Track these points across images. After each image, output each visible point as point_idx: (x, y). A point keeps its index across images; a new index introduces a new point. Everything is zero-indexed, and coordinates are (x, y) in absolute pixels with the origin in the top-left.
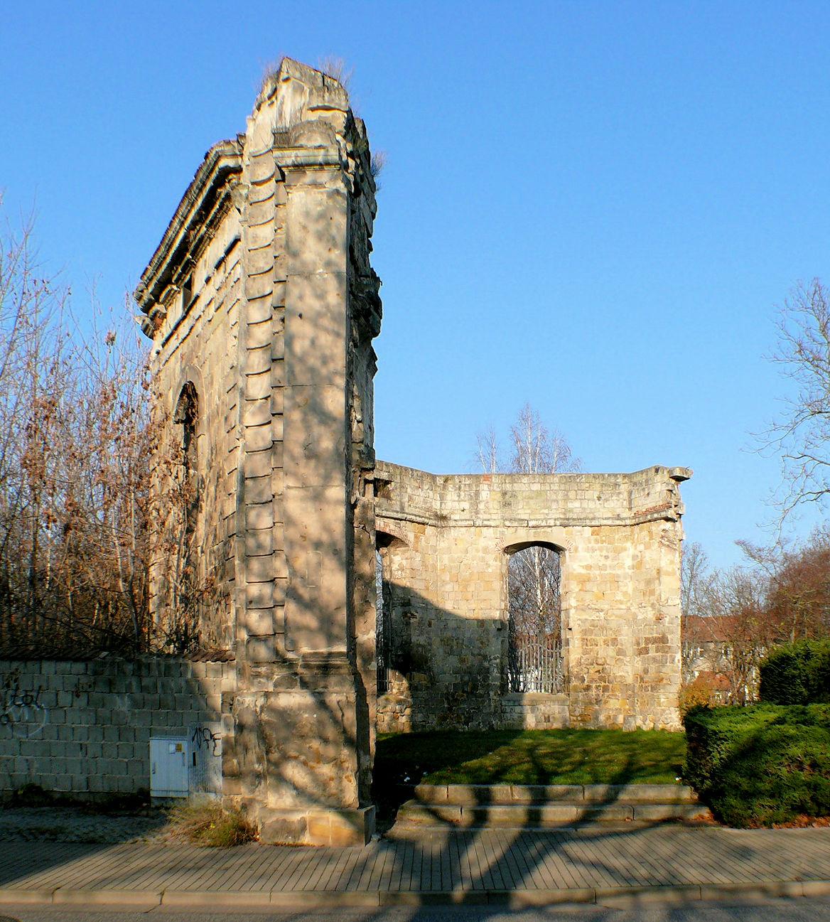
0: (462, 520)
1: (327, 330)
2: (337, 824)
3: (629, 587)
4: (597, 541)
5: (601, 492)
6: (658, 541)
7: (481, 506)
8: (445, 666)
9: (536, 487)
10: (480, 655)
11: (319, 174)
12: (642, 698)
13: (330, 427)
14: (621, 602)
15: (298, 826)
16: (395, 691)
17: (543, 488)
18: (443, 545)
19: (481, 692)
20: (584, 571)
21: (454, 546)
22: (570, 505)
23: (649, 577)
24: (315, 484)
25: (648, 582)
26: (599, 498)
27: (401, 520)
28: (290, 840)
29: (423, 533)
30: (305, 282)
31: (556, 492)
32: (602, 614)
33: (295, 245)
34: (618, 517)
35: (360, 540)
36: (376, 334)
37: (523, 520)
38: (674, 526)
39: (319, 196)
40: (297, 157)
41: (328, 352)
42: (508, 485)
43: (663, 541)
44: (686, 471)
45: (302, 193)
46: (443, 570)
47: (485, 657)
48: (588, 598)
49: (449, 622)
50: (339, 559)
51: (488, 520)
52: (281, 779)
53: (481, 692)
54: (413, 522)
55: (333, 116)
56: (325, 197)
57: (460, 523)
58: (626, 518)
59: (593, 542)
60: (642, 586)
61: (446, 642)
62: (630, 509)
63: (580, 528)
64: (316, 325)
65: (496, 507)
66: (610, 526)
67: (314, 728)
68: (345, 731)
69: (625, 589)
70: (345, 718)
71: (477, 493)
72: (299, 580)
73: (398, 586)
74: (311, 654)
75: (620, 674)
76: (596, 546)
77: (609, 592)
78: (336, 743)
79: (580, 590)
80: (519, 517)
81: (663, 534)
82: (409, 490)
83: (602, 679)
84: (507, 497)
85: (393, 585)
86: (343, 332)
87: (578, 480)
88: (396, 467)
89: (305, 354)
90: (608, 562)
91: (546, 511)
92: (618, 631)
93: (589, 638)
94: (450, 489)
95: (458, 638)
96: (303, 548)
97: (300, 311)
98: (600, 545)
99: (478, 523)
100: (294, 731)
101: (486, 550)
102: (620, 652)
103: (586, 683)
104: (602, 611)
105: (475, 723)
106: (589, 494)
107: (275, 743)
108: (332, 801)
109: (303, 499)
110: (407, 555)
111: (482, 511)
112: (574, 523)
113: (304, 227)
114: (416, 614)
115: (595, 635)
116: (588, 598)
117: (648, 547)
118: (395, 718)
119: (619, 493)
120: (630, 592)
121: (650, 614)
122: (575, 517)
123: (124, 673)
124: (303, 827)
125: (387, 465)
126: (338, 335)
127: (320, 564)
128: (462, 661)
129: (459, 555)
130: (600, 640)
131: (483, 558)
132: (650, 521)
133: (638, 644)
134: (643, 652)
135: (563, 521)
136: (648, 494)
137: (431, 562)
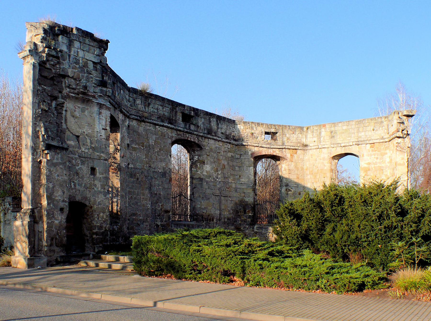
4: (373, 151)
5: (375, 126)
7: (322, 139)
9: (345, 128)
20: (366, 166)
21: (311, 158)
22: (360, 135)
26: (373, 130)
29: (296, 153)
34: (383, 138)
43: (398, 148)
46: (307, 169)
57: (313, 148)
59: (371, 151)
62: (388, 133)
63: (365, 145)
65: (328, 138)
66: (379, 143)
69: (386, 173)
71: (320, 133)
76: (372, 153)
80: (337, 142)
82: (287, 135)
84: (333, 133)
85: (283, 177)
88: (280, 126)
90: (378, 161)
91: (349, 138)
98: (374, 152)
99: (320, 147)
101: (324, 159)
125: (274, 126)
137: (301, 166)
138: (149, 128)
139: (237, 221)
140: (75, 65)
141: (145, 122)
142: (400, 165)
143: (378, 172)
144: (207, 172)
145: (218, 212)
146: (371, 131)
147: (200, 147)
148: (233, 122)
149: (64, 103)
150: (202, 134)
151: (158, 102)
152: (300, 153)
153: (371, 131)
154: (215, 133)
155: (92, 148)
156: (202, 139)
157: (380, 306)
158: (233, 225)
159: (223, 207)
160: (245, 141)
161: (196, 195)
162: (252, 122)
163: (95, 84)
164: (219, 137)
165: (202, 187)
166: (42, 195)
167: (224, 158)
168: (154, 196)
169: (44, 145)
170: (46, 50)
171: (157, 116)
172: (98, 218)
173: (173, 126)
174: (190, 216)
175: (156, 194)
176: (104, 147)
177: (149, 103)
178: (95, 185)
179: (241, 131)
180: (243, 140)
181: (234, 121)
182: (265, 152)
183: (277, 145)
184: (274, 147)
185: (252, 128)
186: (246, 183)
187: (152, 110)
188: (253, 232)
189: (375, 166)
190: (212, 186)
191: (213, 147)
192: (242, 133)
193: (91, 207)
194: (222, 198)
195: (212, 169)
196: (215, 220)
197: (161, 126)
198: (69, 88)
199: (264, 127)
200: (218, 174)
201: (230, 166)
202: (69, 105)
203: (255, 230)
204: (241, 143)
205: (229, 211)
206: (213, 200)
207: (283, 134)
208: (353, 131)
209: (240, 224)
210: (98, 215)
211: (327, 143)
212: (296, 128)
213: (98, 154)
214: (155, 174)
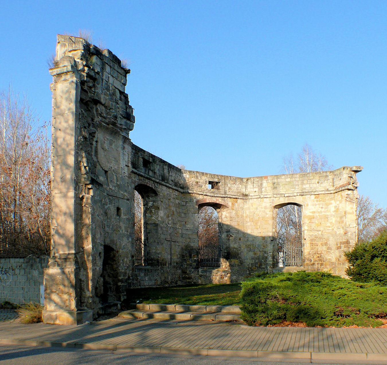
0: (254, 196)
1: (69, 134)
2: (67, 317)
3: (333, 220)
4: (317, 201)
5: (319, 180)
6: (345, 199)
7: (263, 189)
8: (248, 257)
9: (288, 180)
11: (66, 76)
12: (339, 268)
13: (69, 170)
14: (329, 227)
15: (55, 317)
16: (223, 267)
17: (292, 180)
18: (246, 206)
19: (263, 266)
20: (311, 214)
22: (304, 186)
23: (341, 215)
24: (65, 191)
25: (341, 218)
26: (318, 183)
27: (225, 197)
28: (52, 322)
29: (237, 202)
30: (62, 117)
31: (298, 181)
32: (320, 232)
33: (59, 104)
34: (328, 190)
35: (85, 211)
36: (131, 130)
37: (282, 194)
38: (353, 193)
39: (67, 84)
40: (57, 71)
41: (69, 142)
42: (275, 180)
43: (347, 199)
44: (359, 167)
45: (61, 84)
46: (246, 217)
47: (265, 252)
48: (313, 225)
49: (249, 238)
50: (72, 219)
51: (266, 195)
52: (51, 300)
54: (231, 198)
55: (77, 53)
56: (68, 84)
58: (331, 190)
60: (339, 219)
61: (248, 246)
62: (333, 186)
64: (65, 132)
65: (270, 189)
66: (324, 194)
67: (61, 281)
68: (71, 282)
69: (331, 221)
70: (71, 277)
71: (261, 184)
72: (59, 227)
73: (225, 224)
74: (62, 254)
75: (329, 258)
76: (317, 203)
77: (324, 222)
78: (68, 287)
79: (310, 222)
80: (281, 193)
81: (347, 196)
82: (229, 185)
83: (320, 260)
84: (275, 185)
85: (223, 224)
86: (74, 134)
87: (308, 175)
88: (222, 176)
89: (62, 144)
90: (323, 210)
91: (293, 190)
92: (328, 239)
93: (314, 243)
94: (249, 183)
95: (253, 245)
96: (61, 215)
97: (60, 128)
98: (319, 202)
99: (262, 196)
100: (54, 282)
101: (266, 208)
102: (329, 248)
103: (312, 262)
104: (320, 231)
106: (313, 181)
107: (48, 286)
108: (67, 308)
109: (60, 197)
110: (229, 211)
111: (264, 192)
112: (306, 194)
113: (61, 97)
115: (317, 241)
116: (313, 225)
117: (341, 202)
118: (222, 277)
119: (328, 180)
120: (334, 222)
121: (342, 232)
122: (307, 191)
123: (36, 262)
124: (57, 318)
125: (217, 176)
126: (72, 135)
127: (66, 221)
128: (255, 254)
129: (254, 210)
130: (319, 243)
131: (264, 211)
132: (341, 191)
133: (337, 245)
134: (339, 248)
135: (301, 193)
136: (340, 179)
140: (106, 91)
142: (350, 213)
143: (323, 220)
144: (161, 218)
146: (316, 183)
147: (155, 193)
148: (179, 171)
149: (95, 133)
150: (158, 181)
152: (240, 202)
153: (316, 183)
155: (118, 186)
156: (157, 185)
157: (205, 334)
161: (151, 240)
162: (197, 172)
163: (122, 115)
164: (170, 184)
165: (157, 232)
166: (84, 237)
169: (88, 178)
170: (86, 69)
172: (123, 264)
174: (144, 260)
176: (126, 185)
178: (120, 227)
180: (188, 188)
182: (208, 200)
183: (220, 194)
184: (218, 195)
185: (197, 177)
186: (192, 229)
188: (198, 275)
189: (320, 214)
191: (166, 193)
193: (118, 251)
194: (172, 242)
195: (165, 214)
198: (101, 116)
199: (208, 176)
202: (100, 135)
203: (200, 273)
204: (187, 191)
205: (177, 256)
206: (166, 245)
207: (225, 184)
208: (297, 183)
210: (123, 260)
211: (269, 193)
212: (236, 179)
213: (122, 192)
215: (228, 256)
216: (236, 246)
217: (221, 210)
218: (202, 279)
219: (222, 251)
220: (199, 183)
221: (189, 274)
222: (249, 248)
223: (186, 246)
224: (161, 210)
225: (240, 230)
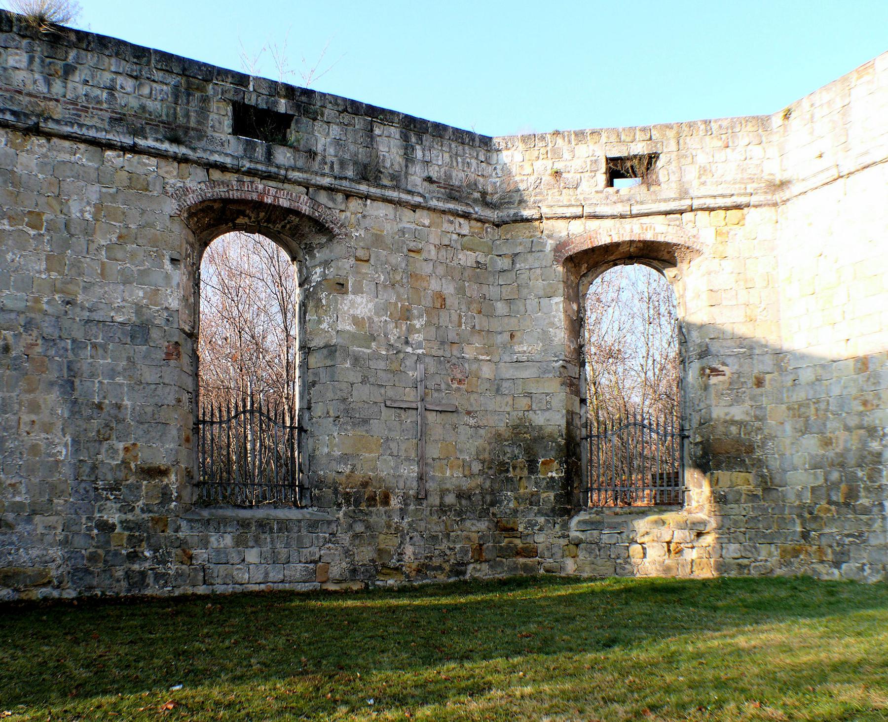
8: (796, 459)
10: (861, 427)
27: (681, 212)
47: (872, 431)
53: (864, 501)
61: (797, 410)
88: (669, 127)
95: (818, 402)
105: (854, 565)
114: (722, 368)
125: (643, 130)
128: (827, 443)
138: (67, 157)
139: (500, 502)
141: (49, 136)
145: (410, 471)
150: (326, 181)
151: (113, 64)
154: (393, 177)
158: (484, 514)
159: (433, 451)
160: (530, 204)
162: (557, 133)
164: (410, 192)
167: (441, 270)
168: (86, 412)
171: (107, 115)
173: (182, 150)
175: (100, 406)
177: (67, 65)
179: (514, 170)
181: (486, 142)
183: (655, 201)
184: (644, 208)
186: (538, 357)
187: (82, 90)
190: (381, 374)
191: (389, 229)
192: (517, 178)
194: (431, 417)
195: (384, 308)
196: (395, 502)
197: (125, 149)
200: (411, 330)
201: (470, 301)
204: (512, 212)
209: (515, 511)
212: (733, 126)
214: (94, 330)
215: (707, 461)
216: (738, 413)
217: (681, 270)
218: (582, 554)
219: (688, 437)
220: (564, 175)
221: (528, 535)
222: (806, 418)
223: (515, 427)
224: (358, 291)
225: (757, 342)
